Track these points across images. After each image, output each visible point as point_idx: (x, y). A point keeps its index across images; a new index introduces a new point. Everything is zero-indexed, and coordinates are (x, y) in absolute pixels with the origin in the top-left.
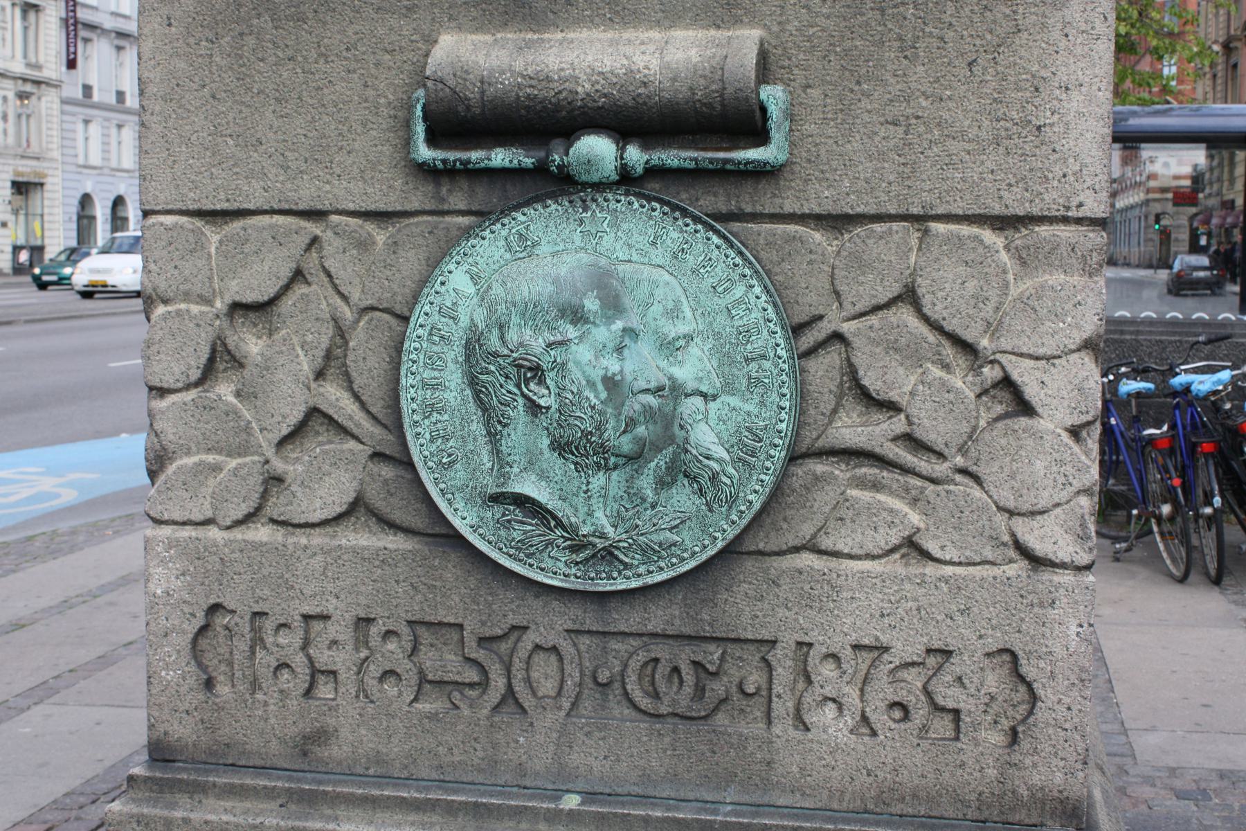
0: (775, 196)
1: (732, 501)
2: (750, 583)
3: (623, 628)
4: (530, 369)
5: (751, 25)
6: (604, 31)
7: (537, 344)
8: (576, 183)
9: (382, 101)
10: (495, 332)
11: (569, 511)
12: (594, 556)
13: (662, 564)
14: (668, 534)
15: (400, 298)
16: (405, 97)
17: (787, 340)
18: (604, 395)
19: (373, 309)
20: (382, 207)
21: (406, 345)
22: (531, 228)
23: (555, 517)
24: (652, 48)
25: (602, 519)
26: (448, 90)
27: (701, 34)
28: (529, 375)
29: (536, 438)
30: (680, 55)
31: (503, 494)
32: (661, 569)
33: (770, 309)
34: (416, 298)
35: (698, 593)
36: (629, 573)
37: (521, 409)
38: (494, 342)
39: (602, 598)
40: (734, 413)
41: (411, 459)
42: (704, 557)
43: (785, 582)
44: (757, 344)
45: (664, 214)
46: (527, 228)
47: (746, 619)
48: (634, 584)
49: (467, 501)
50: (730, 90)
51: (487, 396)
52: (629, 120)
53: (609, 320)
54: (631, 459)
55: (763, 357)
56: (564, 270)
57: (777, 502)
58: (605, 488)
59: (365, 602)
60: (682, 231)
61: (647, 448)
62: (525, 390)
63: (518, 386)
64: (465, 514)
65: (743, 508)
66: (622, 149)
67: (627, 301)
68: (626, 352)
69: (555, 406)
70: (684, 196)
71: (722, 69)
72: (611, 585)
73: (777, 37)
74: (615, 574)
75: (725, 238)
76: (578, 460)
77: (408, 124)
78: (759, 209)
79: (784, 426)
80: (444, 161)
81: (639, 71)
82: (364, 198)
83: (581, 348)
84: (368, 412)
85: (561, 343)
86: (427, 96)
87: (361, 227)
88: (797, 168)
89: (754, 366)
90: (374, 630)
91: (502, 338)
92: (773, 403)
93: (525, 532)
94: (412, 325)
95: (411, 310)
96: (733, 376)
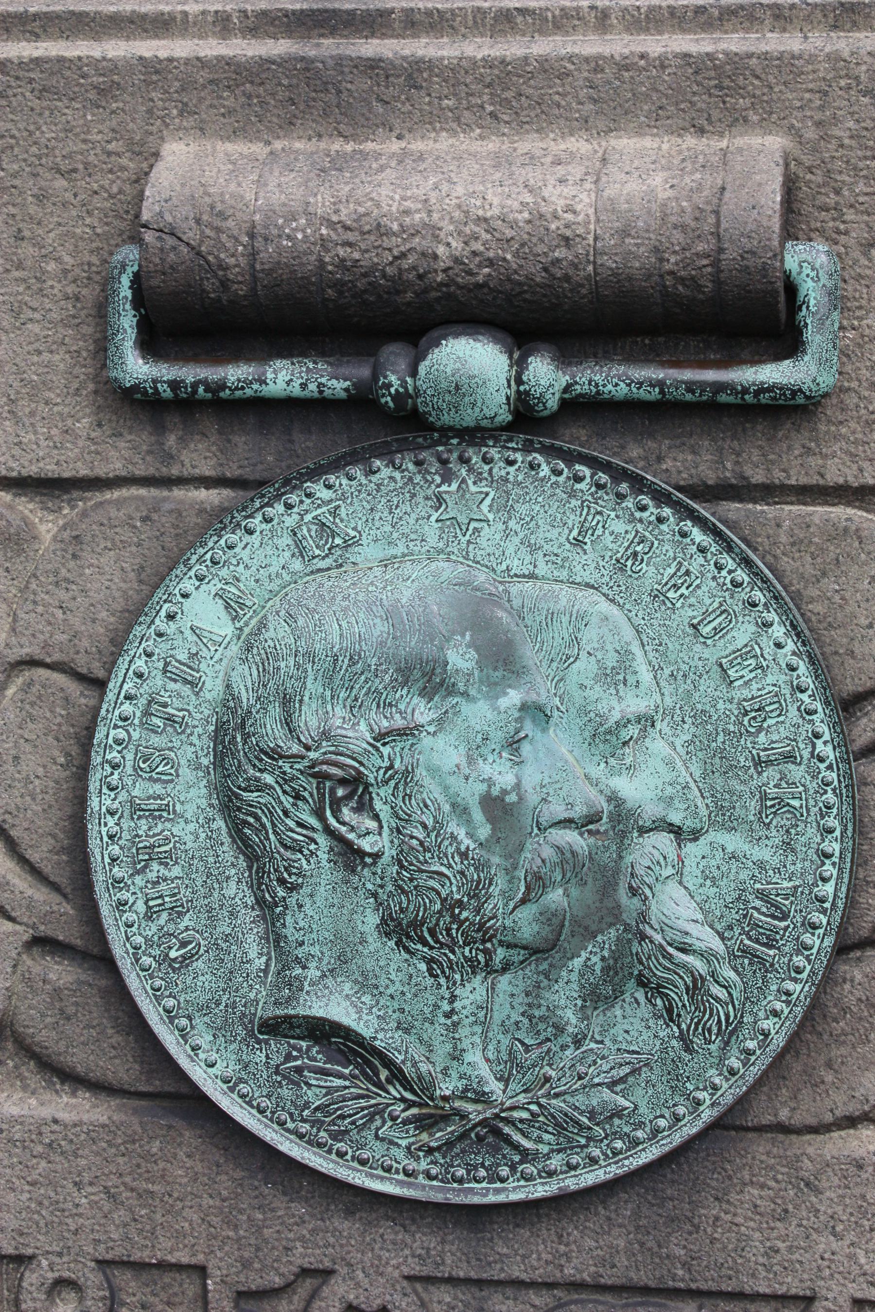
0: (808, 451)
1: (730, 1032)
2: (763, 1186)
3: (517, 1272)
4: (343, 782)
5: (765, 126)
6: (482, 137)
7: (358, 734)
8: (431, 428)
9: (51, 266)
10: (275, 710)
11: (417, 1052)
12: (464, 1136)
13: (596, 1152)
14: (606, 1094)
15: (85, 643)
16: (95, 260)
17: (833, 726)
18: (484, 832)
19: (33, 663)
20: (50, 469)
21: (99, 735)
22: (343, 512)
23: (388, 1063)
24: (576, 171)
25: (479, 1065)
26: (185, 250)
27: (668, 143)
28: (340, 792)
29: (353, 912)
30: (633, 186)
31: (288, 1018)
32: (594, 1161)
33: (803, 668)
34: (118, 643)
35: (661, 1206)
36: (530, 1169)
37: (323, 856)
38: (272, 731)
39: (477, 1217)
40: (734, 865)
41: (109, 950)
42: (677, 1139)
43: (830, 1182)
44: (776, 734)
45: (600, 487)
46: (334, 513)
47: (755, 1253)
48: (541, 1190)
49: (217, 1031)
50: (731, 254)
51: (257, 831)
52: (532, 309)
53: (495, 689)
54: (536, 951)
55: (790, 757)
56: (407, 593)
57: (814, 1031)
58: (486, 1007)
59: (14, 1224)
60: (632, 520)
61: (566, 930)
62: (332, 821)
63: (319, 814)
64: (214, 1056)
65: (751, 1045)
66: (520, 365)
67: (529, 653)
68: (526, 748)
69: (390, 852)
70: (635, 452)
71: (717, 213)
72: (497, 1191)
73: (815, 150)
74: (504, 1171)
75: (716, 533)
76: (435, 954)
77: (102, 312)
78: (778, 476)
79: (829, 889)
80: (174, 385)
81: (556, 217)
82: (16, 451)
83: (440, 742)
84: (23, 861)
85: (403, 733)
86: (144, 258)
87: (10, 507)
88: (851, 400)
89: (771, 774)
90: (31, 1278)
91: (288, 723)
92: (808, 845)
93: (330, 1091)
94: (110, 696)
95: (111, 666)
96: (731, 793)
